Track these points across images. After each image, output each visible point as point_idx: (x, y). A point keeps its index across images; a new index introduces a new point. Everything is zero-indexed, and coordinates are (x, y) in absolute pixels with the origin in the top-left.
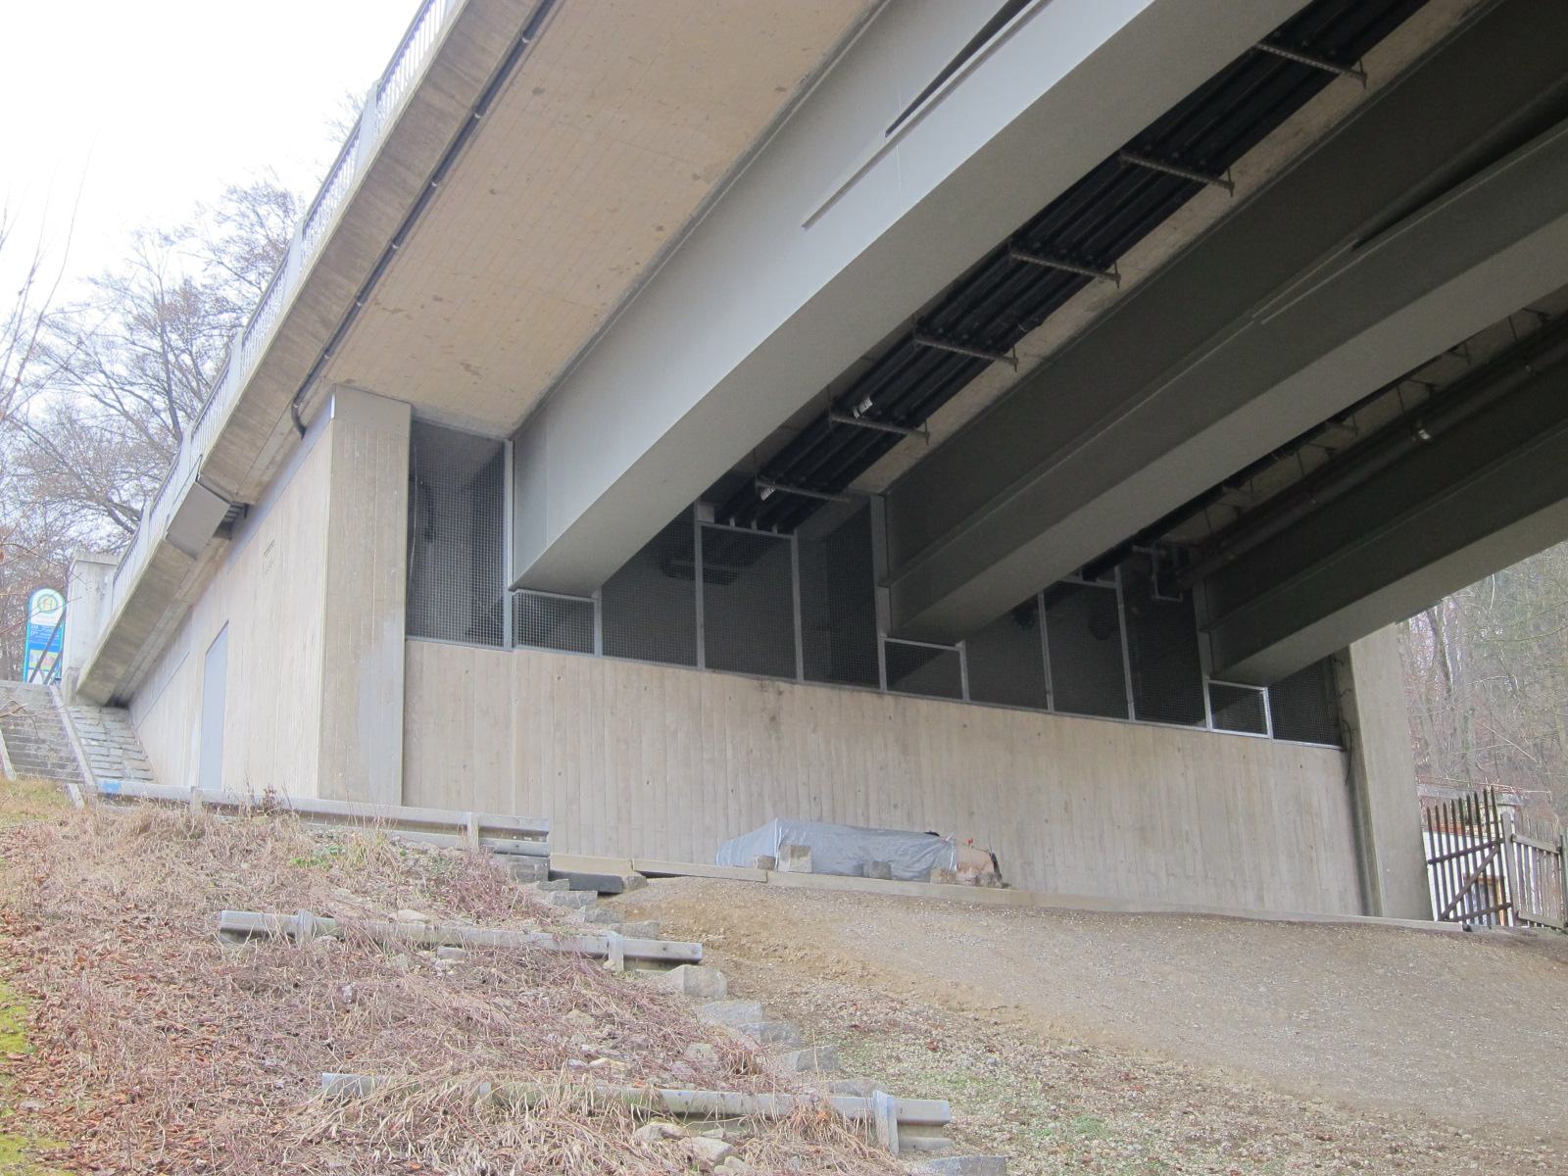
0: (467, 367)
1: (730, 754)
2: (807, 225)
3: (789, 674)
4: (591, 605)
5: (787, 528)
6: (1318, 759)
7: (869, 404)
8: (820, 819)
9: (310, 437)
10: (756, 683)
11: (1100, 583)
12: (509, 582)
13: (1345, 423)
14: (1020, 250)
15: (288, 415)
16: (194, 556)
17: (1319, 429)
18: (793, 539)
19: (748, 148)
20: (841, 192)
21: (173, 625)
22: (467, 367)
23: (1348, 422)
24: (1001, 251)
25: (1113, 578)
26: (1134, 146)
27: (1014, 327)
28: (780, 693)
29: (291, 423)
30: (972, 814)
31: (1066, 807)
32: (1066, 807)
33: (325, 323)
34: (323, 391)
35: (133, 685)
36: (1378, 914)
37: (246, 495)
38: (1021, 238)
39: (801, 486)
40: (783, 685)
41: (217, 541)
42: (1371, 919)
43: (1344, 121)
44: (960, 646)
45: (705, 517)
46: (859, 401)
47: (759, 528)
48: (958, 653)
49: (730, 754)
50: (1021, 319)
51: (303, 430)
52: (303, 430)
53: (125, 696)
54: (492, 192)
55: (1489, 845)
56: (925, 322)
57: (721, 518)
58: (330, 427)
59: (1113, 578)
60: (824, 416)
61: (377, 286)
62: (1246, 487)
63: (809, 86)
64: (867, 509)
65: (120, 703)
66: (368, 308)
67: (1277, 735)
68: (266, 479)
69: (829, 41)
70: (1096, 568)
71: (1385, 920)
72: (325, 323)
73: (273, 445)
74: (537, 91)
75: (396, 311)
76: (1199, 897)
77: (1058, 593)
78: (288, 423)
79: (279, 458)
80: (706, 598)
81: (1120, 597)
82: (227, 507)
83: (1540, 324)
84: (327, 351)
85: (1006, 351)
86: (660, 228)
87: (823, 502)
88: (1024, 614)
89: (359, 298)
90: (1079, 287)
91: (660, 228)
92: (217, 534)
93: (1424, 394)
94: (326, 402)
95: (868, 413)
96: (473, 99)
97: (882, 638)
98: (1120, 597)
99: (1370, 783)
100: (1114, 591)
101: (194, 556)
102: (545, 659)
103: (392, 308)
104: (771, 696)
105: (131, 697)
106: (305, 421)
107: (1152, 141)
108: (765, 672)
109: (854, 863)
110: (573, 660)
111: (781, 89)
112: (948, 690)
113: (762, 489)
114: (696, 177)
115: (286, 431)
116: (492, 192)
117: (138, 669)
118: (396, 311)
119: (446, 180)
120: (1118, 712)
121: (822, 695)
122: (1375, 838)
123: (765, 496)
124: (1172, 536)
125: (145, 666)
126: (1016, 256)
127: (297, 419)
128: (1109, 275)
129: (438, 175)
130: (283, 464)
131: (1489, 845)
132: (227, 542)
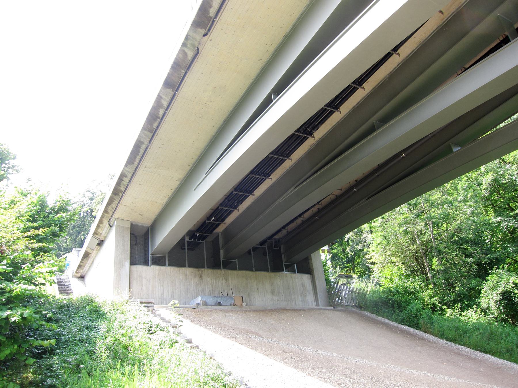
0: (140, 215)
1: (193, 283)
2: (194, 190)
3: (204, 267)
4: (166, 257)
5: (203, 240)
6: (306, 278)
7: (213, 218)
8: (210, 295)
9: (112, 228)
10: (197, 269)
11: (263, 246)
12: (150, 253)
13: (302, 217)
14: (236, 191)
15: (108, 224)
16: (93, 250)
17: (315, 205)
18: (204, 242)
19: (185, 175)
20: (203, 180)
21: (91, 262)
22: (140, 215)
23: (320, 203)
24: (249, 175)
25: (265, 246)
26: (272, 153)
27: (311, 131)
28: (202, 271)
29: (108, 226)
30: (239, 291)
31: (258, 289)
32: (258, 289)
33: (113, 208)
34: (114, 220)
35: (84, 274)
36: (319, 306)
37: (102, 238)
38: (252, 172)
39: (204, 233)
40: (203, 270)
41: (97, 247)
42: (318, 307)
43: (292, 165)
44: (236, 260)
45: (187, 239)
46: (212, 218)
47: (198, 240)
48: (236, 261)
49: (193, 283)
50: (313, 129)
51: (111, 227)
52: (111, 227)
53: (83, 276)
54: (140, 184)
55: (338, 291)
56: (236, 189)
57: (190, 239)
58: (115, 226)
59: (265, 246)
60: (232, 192)
61: (121, 201)
62: (302, 216)
63: (194, 165)
64: (218, 236)
65: (82, 277)
66: (119, 205)
67: (298, 273)
68: (105, 235)
69: (215, 130)
70: (263, 243)
71: (321, 307)
72: (113, 208)
73: (105, 229)
74: (145, 167)
75: (125, 205)
76: (283, 304)
77: (255, 249)
78: (108, 225)
79: (107, 232)
80: (188, 253)
81: (267, 249)
82: (98, 241)
83: (356, 183)
84: (113, 213)
85: (289, 157)
86: (172, 190)
87: (209, 235)
88: (249, 252)
89: (118, 203)
90: (285, 161)
91: (172, 190)
92: (97, 245)
93: (301, 222)
94: (114, 222)
95: (214, 220)
96: (134, 169)
97: (222, 259)
98: (267, 249)
99: (316, 281)
100: (265, 248)
101: (93, 250)
102: (157, 268)
103: (124, 205)
104: (200, 272)
105: (85, 275)
106: (111, 225)
107: (276, 151)
108: (199, 267)
109: (215, 303)
110: (163, 268)
111: (189, 165)
112: (234, 269)
113: (196, 234)
114: (176, 181)
115: (108, 227)
116: (140, 184)
117: (85, 270)
118: (125, 205)
119: (131, 183)
120: (267, 270)
121: (210, 271)
122: (318, 291)
123: (198, 235)
124: (276, 237)
125: (86, 270)
126: (221, 208)
127: (109, 225)
128: (362, 88)
129: (129, 182)
130: (108, 233)
131: (338, 291)
132: (99, 247)
